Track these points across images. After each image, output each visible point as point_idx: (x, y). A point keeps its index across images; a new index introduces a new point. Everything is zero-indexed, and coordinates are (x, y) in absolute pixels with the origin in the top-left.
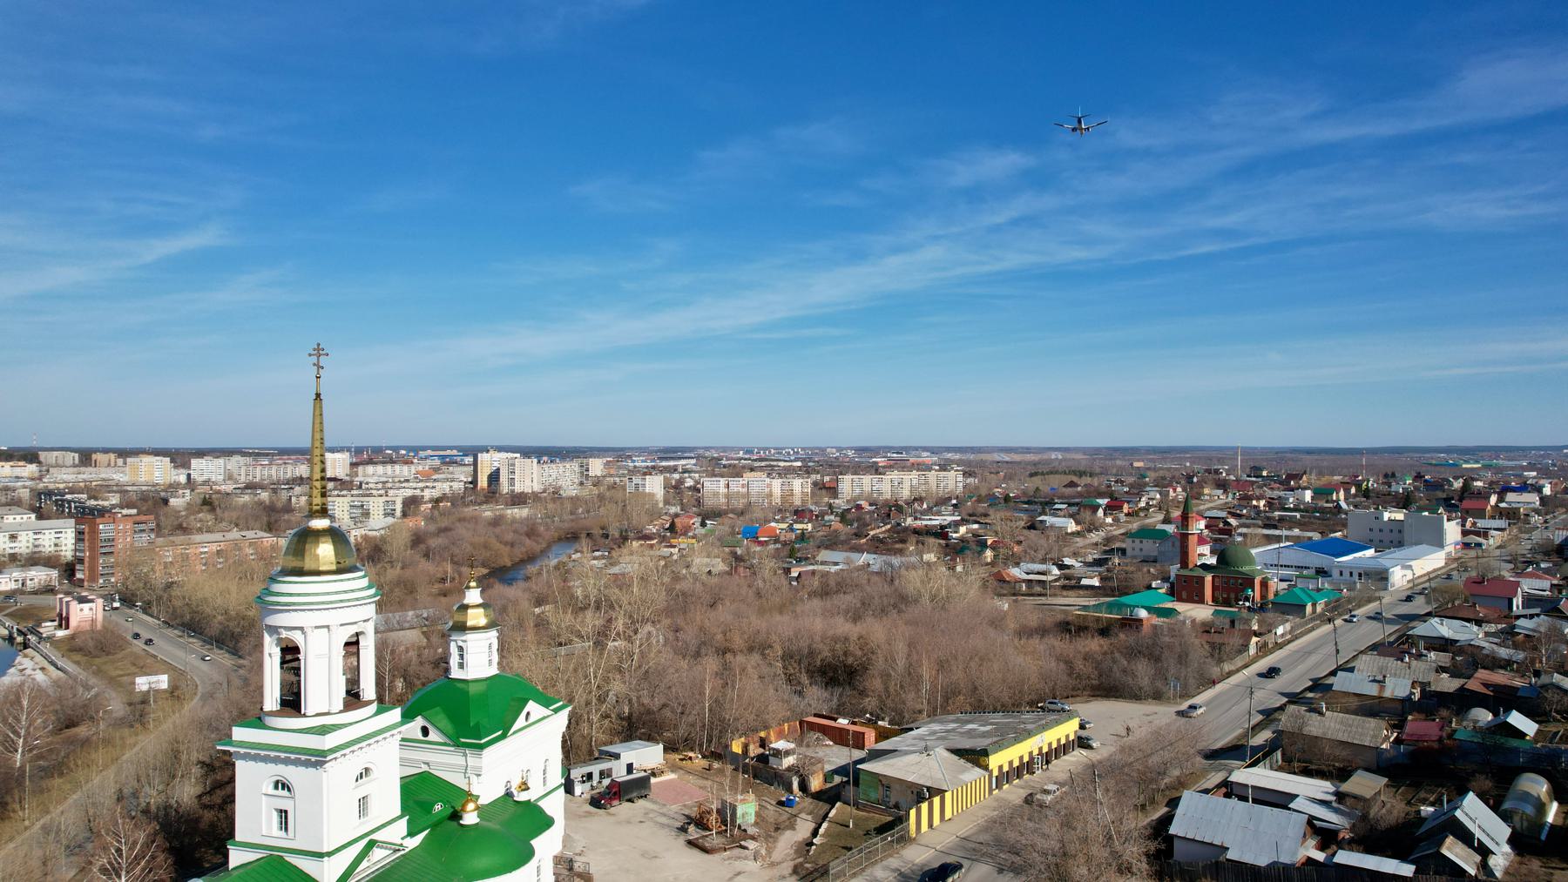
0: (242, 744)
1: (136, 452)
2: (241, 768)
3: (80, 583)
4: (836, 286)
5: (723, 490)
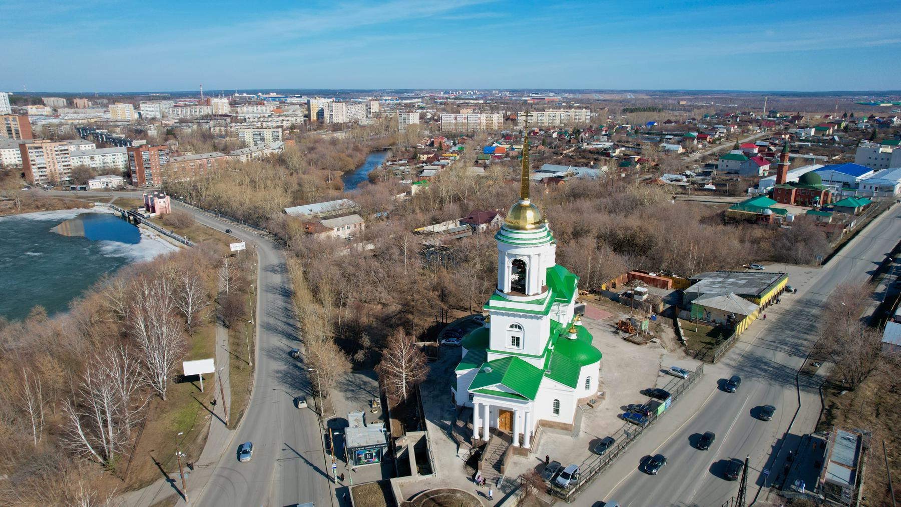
0: (495, 308)
3: (136, 184)
5: (453, 121)
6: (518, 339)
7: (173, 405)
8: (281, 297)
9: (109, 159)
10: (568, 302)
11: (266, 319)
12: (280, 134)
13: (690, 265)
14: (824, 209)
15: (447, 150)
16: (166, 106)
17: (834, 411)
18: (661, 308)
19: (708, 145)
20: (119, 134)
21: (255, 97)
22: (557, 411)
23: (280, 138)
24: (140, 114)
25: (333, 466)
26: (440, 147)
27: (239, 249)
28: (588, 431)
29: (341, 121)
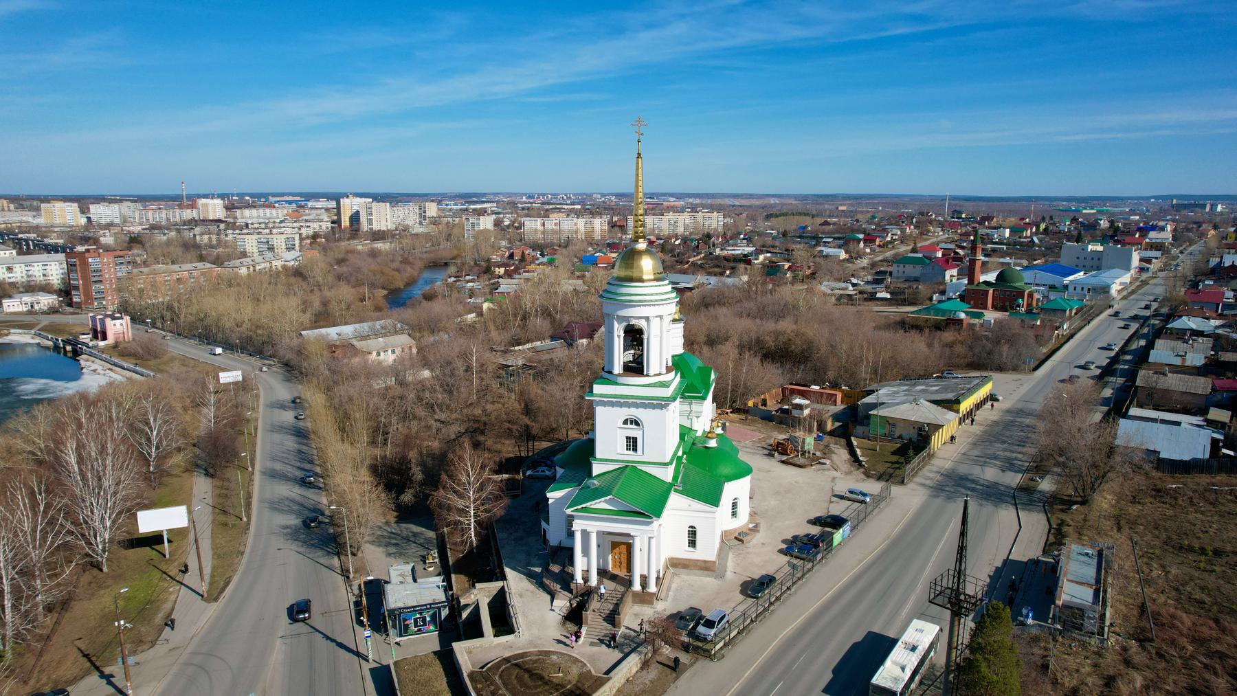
0: (601, 395)
1: (47, 199)
2: (600, 412)
3: (79, 305)
4: (596, 57)
5: (540, 228)
6: (635, 440)
7: (119, 578)
8: (293, 438)
9: (37, 272)
10: (704, 398)
11: (269, 464)
12: (297, 242)
13: (864, 373)
14: (1029, 312)
15: (532, 262)
16: (127, 207)
17: (1065, 529)
18: (829, 426)
19: (878, 249)
20: (52, 240)
21: (261, 200)
22: (692, 543)
23: (297, 247)
24: (89, 219)
25: (366, 638)
26: (523, 258)
27: (231, 380)
28: (738, 569)
29: (383, 228)
